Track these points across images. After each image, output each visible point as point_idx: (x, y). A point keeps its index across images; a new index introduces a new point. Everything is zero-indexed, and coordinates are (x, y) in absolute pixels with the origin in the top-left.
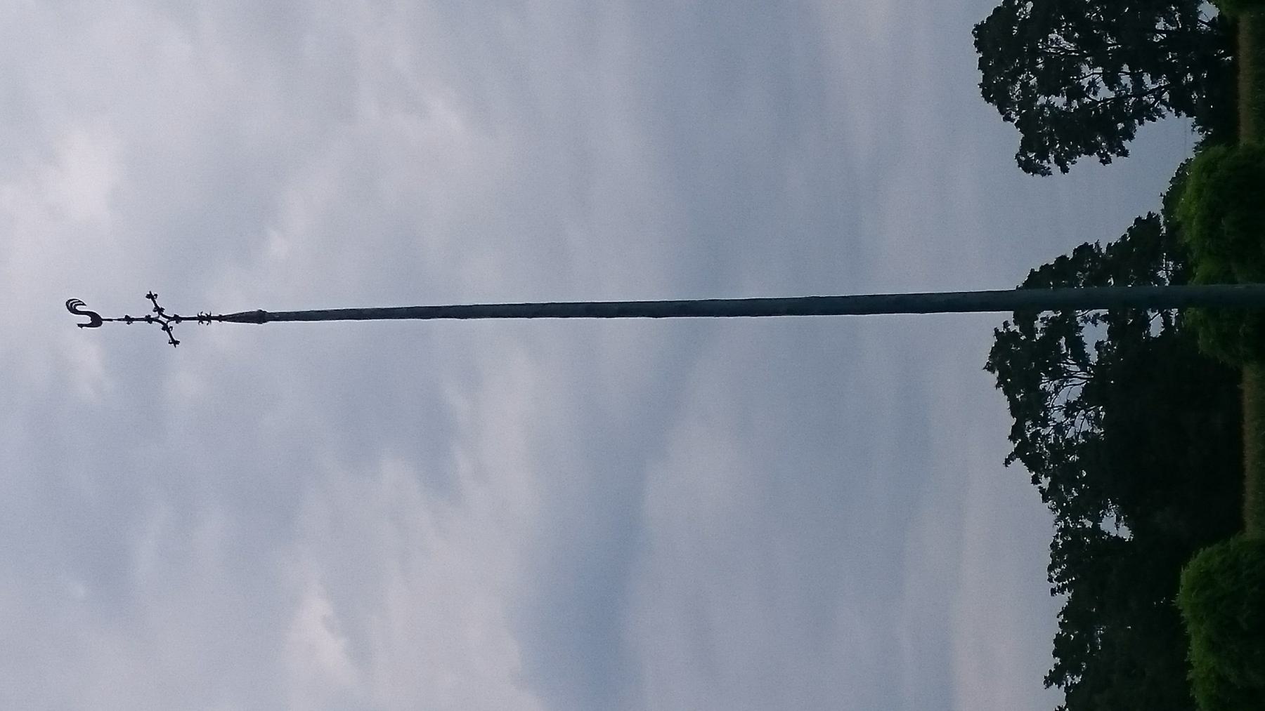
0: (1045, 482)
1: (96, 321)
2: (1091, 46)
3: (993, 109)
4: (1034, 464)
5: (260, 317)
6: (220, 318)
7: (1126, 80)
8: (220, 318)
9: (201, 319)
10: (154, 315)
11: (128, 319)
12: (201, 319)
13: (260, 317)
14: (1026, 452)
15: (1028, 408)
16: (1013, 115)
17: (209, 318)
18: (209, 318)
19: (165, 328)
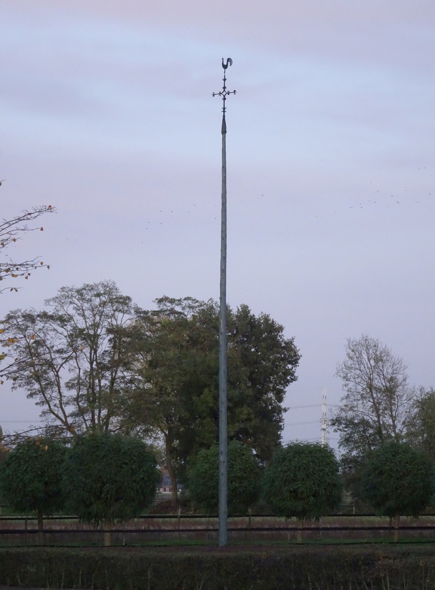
1: (225, 67)
3: (55, 293)
5: (224, 131)
6: (224, 116)
8: (224, 116)
9: (224, 108)
11: (225, 80)
12: (224, 108)
13: (224, 131)
17: (224, 111)
18: (224, 111)
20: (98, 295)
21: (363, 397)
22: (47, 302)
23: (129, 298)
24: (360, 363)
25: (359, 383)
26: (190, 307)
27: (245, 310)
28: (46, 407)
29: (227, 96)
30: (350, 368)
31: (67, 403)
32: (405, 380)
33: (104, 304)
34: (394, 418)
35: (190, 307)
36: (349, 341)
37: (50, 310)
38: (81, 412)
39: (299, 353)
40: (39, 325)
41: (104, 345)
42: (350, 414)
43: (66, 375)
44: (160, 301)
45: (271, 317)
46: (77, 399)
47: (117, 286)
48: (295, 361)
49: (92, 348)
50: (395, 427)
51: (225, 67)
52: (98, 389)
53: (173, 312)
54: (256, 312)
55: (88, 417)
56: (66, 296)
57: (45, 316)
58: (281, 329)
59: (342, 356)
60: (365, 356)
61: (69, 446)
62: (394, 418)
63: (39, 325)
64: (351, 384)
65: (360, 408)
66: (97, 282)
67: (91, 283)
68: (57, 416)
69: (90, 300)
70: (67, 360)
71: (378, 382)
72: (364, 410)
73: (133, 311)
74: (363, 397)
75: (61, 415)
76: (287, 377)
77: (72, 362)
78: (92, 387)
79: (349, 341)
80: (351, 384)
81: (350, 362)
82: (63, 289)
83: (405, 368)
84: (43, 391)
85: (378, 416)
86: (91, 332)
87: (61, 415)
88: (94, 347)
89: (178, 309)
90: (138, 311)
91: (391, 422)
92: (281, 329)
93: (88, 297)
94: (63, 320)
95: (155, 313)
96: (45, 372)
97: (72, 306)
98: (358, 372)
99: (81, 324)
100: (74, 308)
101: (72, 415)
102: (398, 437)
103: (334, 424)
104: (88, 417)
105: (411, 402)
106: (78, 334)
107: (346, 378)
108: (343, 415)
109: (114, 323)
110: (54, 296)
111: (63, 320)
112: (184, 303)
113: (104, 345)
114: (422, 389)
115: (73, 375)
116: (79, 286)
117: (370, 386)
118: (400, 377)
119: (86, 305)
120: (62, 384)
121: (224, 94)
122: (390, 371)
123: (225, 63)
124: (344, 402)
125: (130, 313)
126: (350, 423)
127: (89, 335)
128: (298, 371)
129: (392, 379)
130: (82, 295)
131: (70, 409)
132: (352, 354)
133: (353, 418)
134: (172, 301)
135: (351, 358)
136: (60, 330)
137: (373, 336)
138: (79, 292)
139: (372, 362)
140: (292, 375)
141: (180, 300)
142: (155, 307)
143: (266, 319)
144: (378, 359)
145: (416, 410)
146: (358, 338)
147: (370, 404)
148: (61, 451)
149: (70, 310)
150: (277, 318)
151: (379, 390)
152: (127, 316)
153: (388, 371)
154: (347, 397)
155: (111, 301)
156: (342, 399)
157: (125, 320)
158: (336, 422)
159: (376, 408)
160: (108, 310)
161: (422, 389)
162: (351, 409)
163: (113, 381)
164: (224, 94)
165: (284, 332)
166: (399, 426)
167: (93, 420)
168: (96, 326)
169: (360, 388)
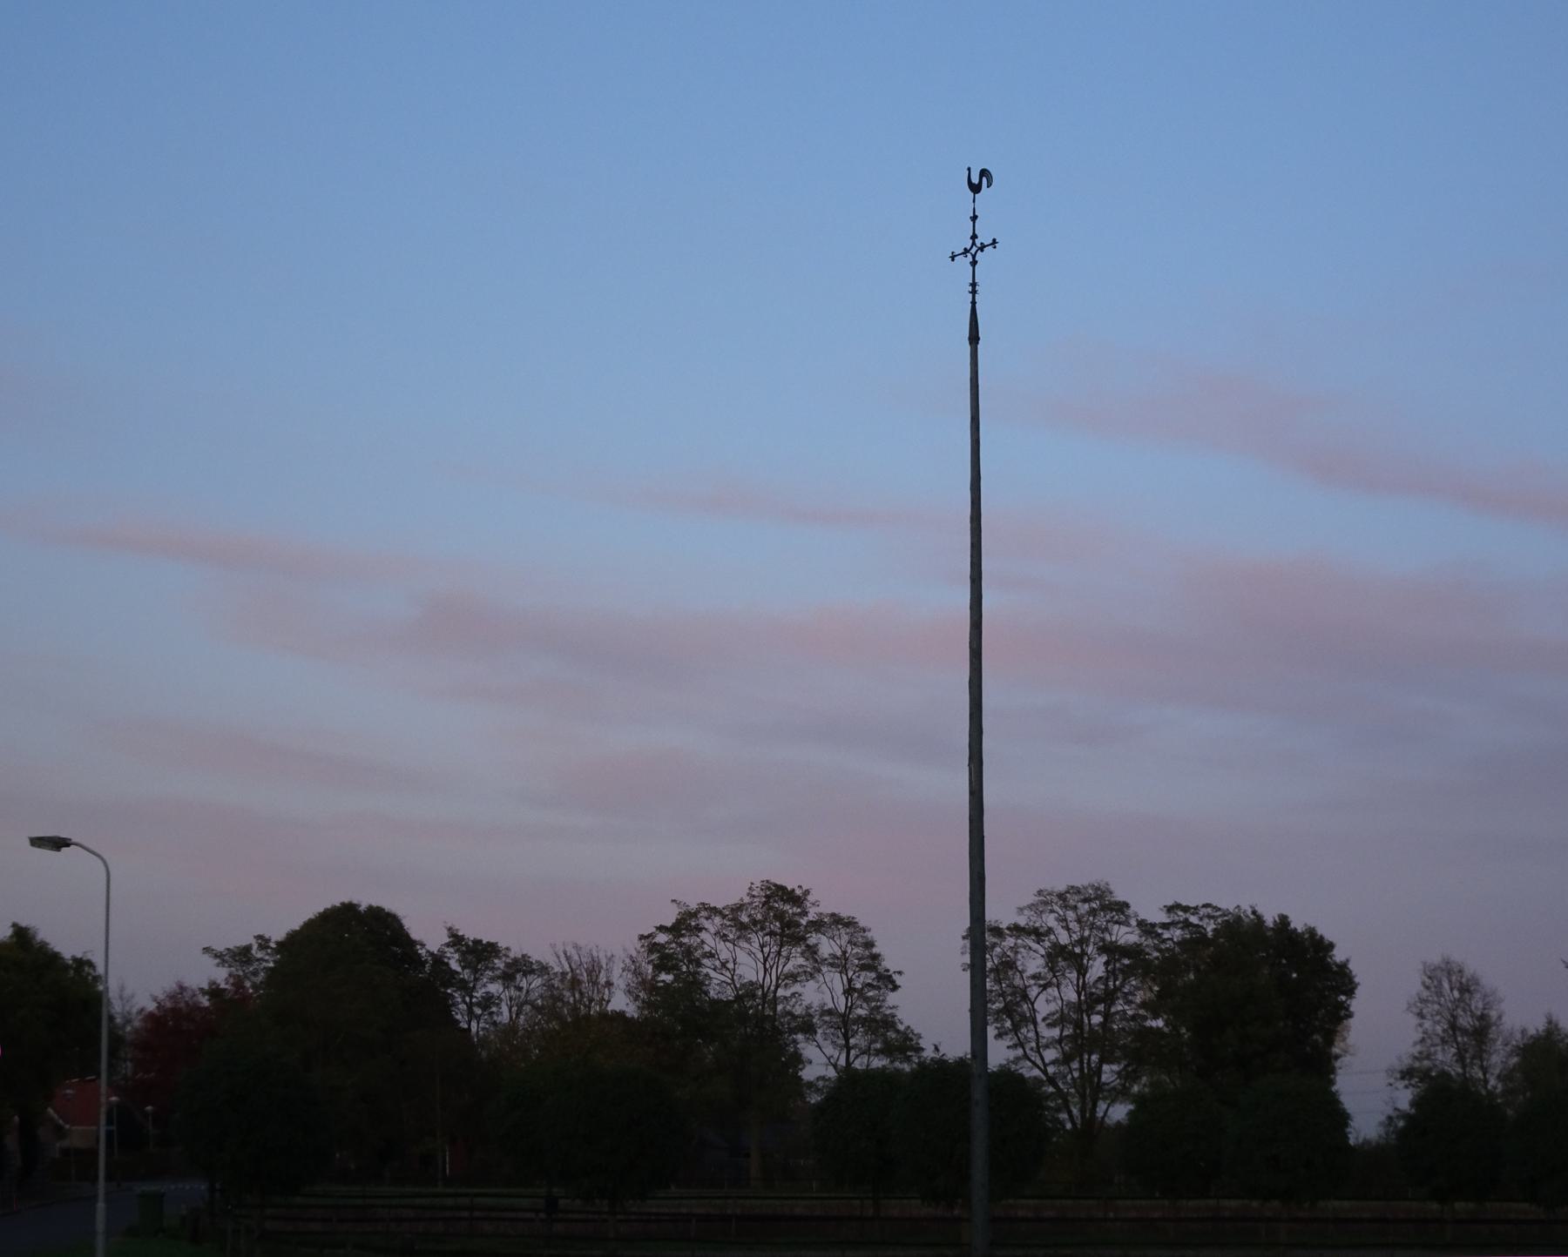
0: (662, 938)
1: (975, 189)
2: (1088, 1002)
3: (1031, 899)
4: (675, 930)
5: (974, 338)
6: (974, 303)
7: (1056, 1032)
8: (974, 303)
9: (974, 285)
10: (978, 242)
11: (974, 218)
12: (974, 285)
13: (974, 338)
14: (685, 924)
15: (737, 922)
16: (1156, 954)
17: (974, 292)
18: (974, 292)
19: (966, 251)
20: (1085, 901)
21: (1444, 1041)
22: (1021, 910)
23: (1127, 905)
24: (1440, 994)
25: (1439, 1022)
26: (1209, 917)
27: (1284, 920)
28: (1020, 1052)
29: (968, 244)
30: (1423, 1001)
31: (1047, 1047)
32: (1500, 1017)
33: (1093, 912)
34: (1485, 1070)
35: (1209, 917)
36: (1424, 964)
37: (1022, 922)
38: (1066, 1059)
39: (1356, 980)
40: (1010, 941)
41: (1097, 968)
42: (1426, 1063)
43: (1044, 1006)
44: (1170, 909)
45: (1319, 932)
46: (1060, 1041)
47: (1112, 888)
48: (1350, 992)
49: (1079, 973)
50: (1486, 1081)
51: (975, 189)
52: (1087, 1028)
53: (1186, 924)
54: (1298, 924)
55: (1075, 1065)
56: (1044, 901)
57: (1017, 930)
58: (1331, 946)
59: (1414, 985)
60: (1446, 985)
61: (484, 1054)
62: (1485, 1070)
63: (1010, 941)
64: (1428, 1024)
65: (1440, 1056)
66: (1086, 883)
67: (1078, 884)
68: (1034, 1063)
69: (1075, 908)
70: (1045, 987)
71: (1465, 1021)
72: (1445, 1057)
73: (1133, 923)
74: (1444, 1041)
75: (1039, 1062)
76: (1340, 1014)
77: (1053, 991)
78: (1078, 1025)
79: (1424, 964)
80: (1428, 1024)
81: (1425, 994)
82: (1040, 893)
83: (1501, 1001)
84: (1016, 1028)
85: (1464, 1067)
86: (1077, 950)
87: (1039, 1062)
88: (1082, 971)
89: (1194, 920)
90: (1142, 924)
91: (1480, 1075)
92: (1331, 946)
93: (1072, 903)
94: (1038, 934)
95: (1165, 926)
96: (1018, 1004)
97: (1053, 915)
98: (1436, 1007)
99: (1064, 938)
100: (1057, 919)
101: (1053, 1062)
102: (1491, 1094)
103: (1403, 1078)
104: (1075, 1065)
105: (1508, 1048)
106: (1057, 954)
107: (1421, 1015)
108: (1417, 1064)
109: (1108, 937)
110: (1030, 901)
111: (1038, 934)
112: (1203, 912)
113: (1097, 968)
114: (1524, 1032)
115: (1053, 1007)
116: (1062, 888)
117: (1453, 1026)
118: (1493, 1014)
119: (1071, 915)
120: (1039, 1018)
121: (974, 250)
122: (1480, 1005)
123: (975, 180)
124: (1418, 1048)
125: (1128, 925)
126: (1425, 1075)
127: (1073, 954)
128: (1356, 1005)
129: (1483, 1017)
130: (1065, 900)
131: (1051, 1054)
132: (1428, 981)
133: (1430, 1070)
134: (1186, 909)
135: (1428, 988)
136: (1035, 946)
137: (1457, 957)
138: (1061, 896)
139: (1456, 994)
140: (1347, 1009)
141: (1196, 908)
142: (1163, 918)
143: (1312, 932)
144: (1465, 989)
145: (1515, 1060)
146: (1436, 959)
147: (1453, 1050)
148: (818, 1090)
149: (1050, 920)
150: (1326, 931)
151: (1465, 1032)
152: (1124, 929)
153: (1477, 1004)
154: (1423, 1041)
155: (1104, 908)
156: (1415, 1044)
157: (1126, 935)
158: (1407, 1074)
159: (1460, 1058)
160: (1101, 921)
161: (1524, 1032)
162: (1428, 1057)
163: (1107, 1016)
164: (974, 250)
165: (1335, 952)
166: (1492, 1082)
167: (1081, 1069)
168: (1083, 941)
169: (1439, 1029)
